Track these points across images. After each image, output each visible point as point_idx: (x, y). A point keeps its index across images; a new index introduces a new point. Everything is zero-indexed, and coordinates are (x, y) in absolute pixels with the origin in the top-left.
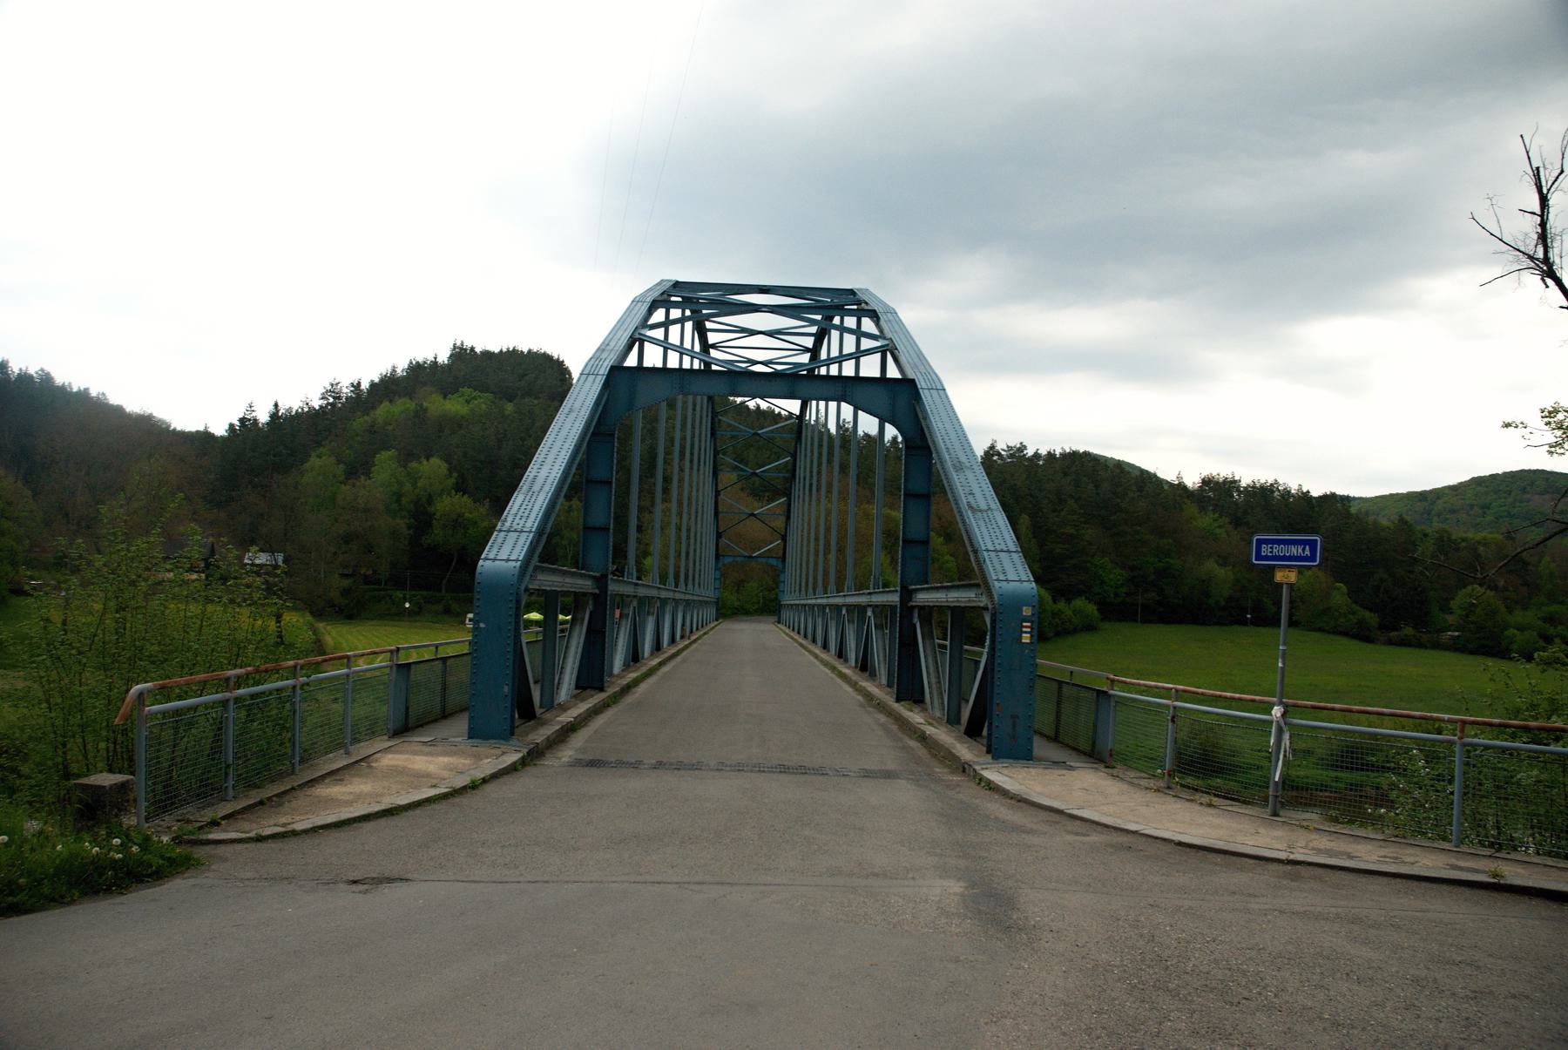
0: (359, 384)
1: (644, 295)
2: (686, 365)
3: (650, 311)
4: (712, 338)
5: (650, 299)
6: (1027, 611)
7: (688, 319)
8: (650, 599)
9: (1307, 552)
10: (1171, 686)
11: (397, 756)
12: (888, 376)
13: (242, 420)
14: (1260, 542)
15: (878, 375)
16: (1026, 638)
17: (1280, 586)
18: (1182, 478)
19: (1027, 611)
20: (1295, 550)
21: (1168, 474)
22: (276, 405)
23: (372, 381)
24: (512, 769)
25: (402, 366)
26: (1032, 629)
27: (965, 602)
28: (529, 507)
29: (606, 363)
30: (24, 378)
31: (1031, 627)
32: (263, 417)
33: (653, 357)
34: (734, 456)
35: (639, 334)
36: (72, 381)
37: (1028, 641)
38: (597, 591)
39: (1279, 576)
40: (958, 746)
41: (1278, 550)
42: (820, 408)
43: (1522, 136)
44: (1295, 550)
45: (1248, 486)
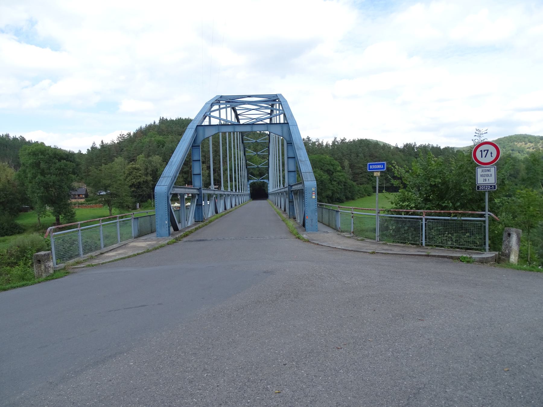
0: (130, 134)
1: (209, 101)
3: (212, 105)
4: (239, 112)
5: (211, 103)
6: (313, 189)
7: (229, 107)
8: (228, 195)
9: (382, 167)
10: (351, 207)
11: (134, 243)
17: (375, 177)
18: (397, 145)
19: (313, 189)
20: (379, 167)
21: (393, 144)
22: (102, 142)
25: (144, 126)
29: (195, 124)
30: (15, 139)
31: (315, 195)
32: (98, 146)
33: (215, 122)
34: (253, 149)
35: (207, 114)
36: (32, 139)
38: (199, 193)
39: (375, 174)
40: (4, 238)
41: (375, 167)
44: (379, 167)
45: (419, 146)
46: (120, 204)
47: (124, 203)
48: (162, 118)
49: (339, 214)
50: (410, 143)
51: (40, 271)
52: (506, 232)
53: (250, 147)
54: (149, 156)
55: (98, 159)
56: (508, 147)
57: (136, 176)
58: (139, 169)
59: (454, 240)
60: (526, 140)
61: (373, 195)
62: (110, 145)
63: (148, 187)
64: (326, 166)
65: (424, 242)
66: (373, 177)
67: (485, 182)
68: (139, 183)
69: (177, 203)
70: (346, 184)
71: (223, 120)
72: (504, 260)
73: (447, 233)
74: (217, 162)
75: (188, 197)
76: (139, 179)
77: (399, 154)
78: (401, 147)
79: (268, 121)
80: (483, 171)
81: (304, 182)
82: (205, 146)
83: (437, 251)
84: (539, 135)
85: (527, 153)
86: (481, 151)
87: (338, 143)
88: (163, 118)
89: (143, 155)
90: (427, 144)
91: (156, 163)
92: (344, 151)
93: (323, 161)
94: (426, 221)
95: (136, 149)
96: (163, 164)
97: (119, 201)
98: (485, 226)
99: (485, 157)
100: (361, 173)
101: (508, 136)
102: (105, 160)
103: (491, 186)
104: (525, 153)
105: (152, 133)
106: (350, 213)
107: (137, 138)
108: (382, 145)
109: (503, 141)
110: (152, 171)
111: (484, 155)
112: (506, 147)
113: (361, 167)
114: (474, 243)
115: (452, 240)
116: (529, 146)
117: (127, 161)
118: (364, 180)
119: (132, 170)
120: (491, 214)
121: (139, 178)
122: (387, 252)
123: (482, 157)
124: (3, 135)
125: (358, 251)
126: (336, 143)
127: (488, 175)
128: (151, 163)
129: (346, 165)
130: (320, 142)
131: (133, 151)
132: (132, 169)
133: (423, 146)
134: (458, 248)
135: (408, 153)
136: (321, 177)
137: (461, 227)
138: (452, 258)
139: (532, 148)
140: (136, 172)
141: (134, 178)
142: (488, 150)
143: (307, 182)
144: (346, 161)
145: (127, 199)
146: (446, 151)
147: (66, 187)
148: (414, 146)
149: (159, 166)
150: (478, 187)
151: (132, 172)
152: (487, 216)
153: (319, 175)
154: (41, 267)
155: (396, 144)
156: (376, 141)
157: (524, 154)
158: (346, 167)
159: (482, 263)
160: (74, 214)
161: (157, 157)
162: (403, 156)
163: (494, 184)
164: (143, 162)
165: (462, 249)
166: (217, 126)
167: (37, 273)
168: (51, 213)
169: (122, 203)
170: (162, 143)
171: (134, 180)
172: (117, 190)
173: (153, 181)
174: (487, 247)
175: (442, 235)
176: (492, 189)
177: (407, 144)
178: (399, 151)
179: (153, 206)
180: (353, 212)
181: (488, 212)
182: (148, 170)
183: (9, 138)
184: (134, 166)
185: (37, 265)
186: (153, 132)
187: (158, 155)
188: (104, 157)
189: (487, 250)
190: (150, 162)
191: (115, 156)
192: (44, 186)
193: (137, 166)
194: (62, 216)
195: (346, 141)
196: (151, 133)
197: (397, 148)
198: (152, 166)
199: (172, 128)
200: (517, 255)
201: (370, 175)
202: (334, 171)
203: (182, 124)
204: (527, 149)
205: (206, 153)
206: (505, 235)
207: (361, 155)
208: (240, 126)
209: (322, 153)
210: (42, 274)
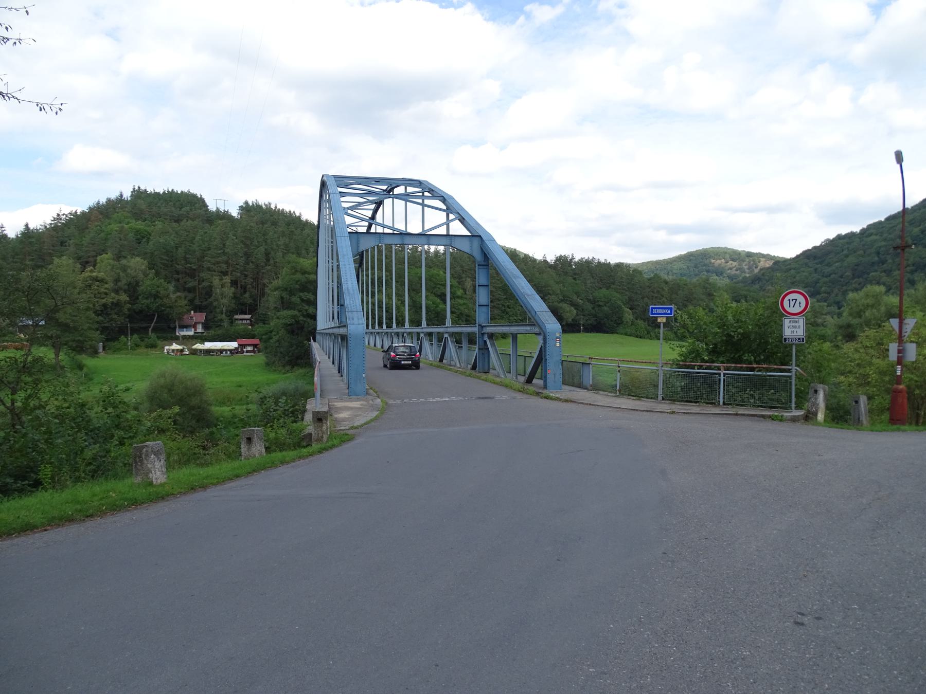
9: (669, 312)
12: (450, 234)
14: (652, 308)
15: (445, 233)
18: (546, 258)
20: (665, 311)
22: (27, 226)
24: (613, 396)
25: (103, 200)
39: (659, 320)
41: (658, 311)
43: (899, 157)
44: (665, 311)
45: (580, 260)
46: (77, 344)
47: (85, 343)
48: (137, 188)
49: (591, 367)
50: (565, 255)
51: (320, 432)
52: (812, 388)
53: (307, 249)
54: (118, 257)
55: (17, 258)
56: (702, 266)
57: (99, 293)
58: (104, 281)
59: (757, 398)
60: (727, 256)
62: (43, 233)
63: (120, 314)
64: (439, 288)
65: (721, 400)
66: (510, 308)
67: (793, 334)
68: (105, 305)
69: (176, 344)
70: (468, 318)
71: (388, 227)
72: (811, 419)
73: (748, 390)
74: (249, 274)
75: (195, 333)
76: (103, 298)
77: (549, 271)
78: (552, 260)
80: (790, 322)
83: (742, 410)
84: (745, 250)
85: (728, 276)
86: (789, 300)
88: (139, 187)
89: (109, 255)
90: (591, 258)
91: (135, 271)
92: (464, 264)
93: (434, 280)
94: (724, 376)
96: (149, 274)
97: (77, 339)
98: (791, 382)
99: (794, 306)
103: (799, 339)
104: (726, 276)
105: (122, 214)
106: (615, 366)
107: (91, 222)
108: (522, 256)
109: (695, 257)
110: (128, 285)
111: (792, 305)
112: (698, 265)
114: (778, 401)
115: (754, 398)
116: (731, 266)
118: (496, 312)
119: (90, 282)
120: (798, 369)
121: (103, 296)
122: (687, 411)
123: (790, 307)
125: (652, 411)
127: (796, 327)
129: (468, 287)
131: (86, 247)
133: (584, 260)
134: (761, 406)
135: (563, 272)
136: (437, 307)
137: (760, 384)
138: (763, 416)
139: (735, 268)
140: (98, 286)
142: (796, 300)
143: (548, 325)
144: (469, 280)
146: (619, 270)
148: (571, 260)
149: (141, 276)
150: (785, 340)
152: (794, 371)
153: (433, 303)
154: (322, 426)
155: (545, 255)
156: (514, 250)
157: (724, 277)
158: (467, 290)
159: (794, 421)
161: (138, 259)
162: (554, 275)
163: (802, 337)
164: (109, 267)
165: (765, 407)
167: (316, 434)
170: (145, 234)
172: (74, 318)
173: (130, 304)
174: (793, 406)
175: (743, 393)
176: (800, 342)
177: (561, 256)
178: (549, 268)
179: (130, 348)
180: (620, 365)
181: (795, 366)
184: (94, 274)
185: (316, 425)
186: (123, 213)
188: (29, 255)
189: (793, 408)
190: (124, 269)
193: (101, 275)
196: (120, 214)
197: (545, 261)
200: (824, 413)
201: (505, 304)
203: (177, 202)
204: (728, 270)
205: (230, 257)
206: (811, 392)
209: (430, 266)
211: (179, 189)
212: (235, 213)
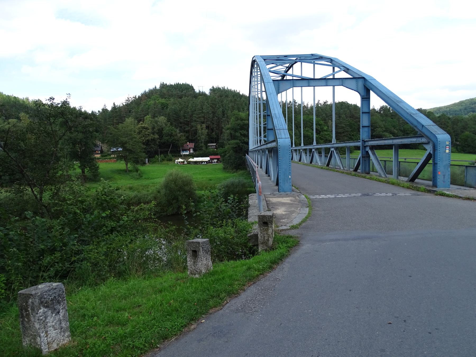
2: (260, 80)
13: (103, 110)
16: (447, 151)
19: (447, 143)
23: (139, 96)
25: (147, 90)
26: (449, 148)
27: (410, 142)
28: (280, 122)
31: (449, 149)
32: (109, 108)
37: (448, 152)
42: (263, 96)
48: (162, 83)
51: (266, 235)
56: (470, 109)
57: (145, 134)
61: (354, 152)
68: (148, 140)
75: (189, 153)
76: (147, 137)
77: (376, 115)
79: (331, 77)
81: (277, 140)
82: (204, 107)
87: (321, 105)
88: (163, 83)
95: (143, 111)
100: (343, 133)
101: (469, 99)
102: (117, 120)
109: (465, 103)
110: (158, 130)
113: (343, 127)
117: (136, 121)
119: (141, 129)
121: (147, 136)
124: (23, 98)
126: (320, 105)
128: (157, 123)
130: (305, 104)
131: (140, 112)
132: (141, 128)
140: (145, 131)
141: (143, 137)
143: (438, 135)
145: (141, 155)
147: (91, 144)
149: (164, 125)
151: (141, 131)
160: (98, 167)
161: (162, 117)
164: (150, 122)
166: (292, 81)
167: (261, 237)
168: (78, 166)
169: (137, 158)
171: (144, 138)
182: (154, 130)
183: (29, 101)
184: (143, 125)
187: (162, 116)
188: (115, 118)
190: (156, 122)
191: (124, 117)
192: (72, 143)
193: (146, 125)
194: (87, 169)
195: (328, 103)
198: (158, 126)
199: (172, 92)
202: (321, 130)
207: (343, 116)
208: (315, 81)
210: (268, 239)
211: (181, 82)
212: (208, 92)
